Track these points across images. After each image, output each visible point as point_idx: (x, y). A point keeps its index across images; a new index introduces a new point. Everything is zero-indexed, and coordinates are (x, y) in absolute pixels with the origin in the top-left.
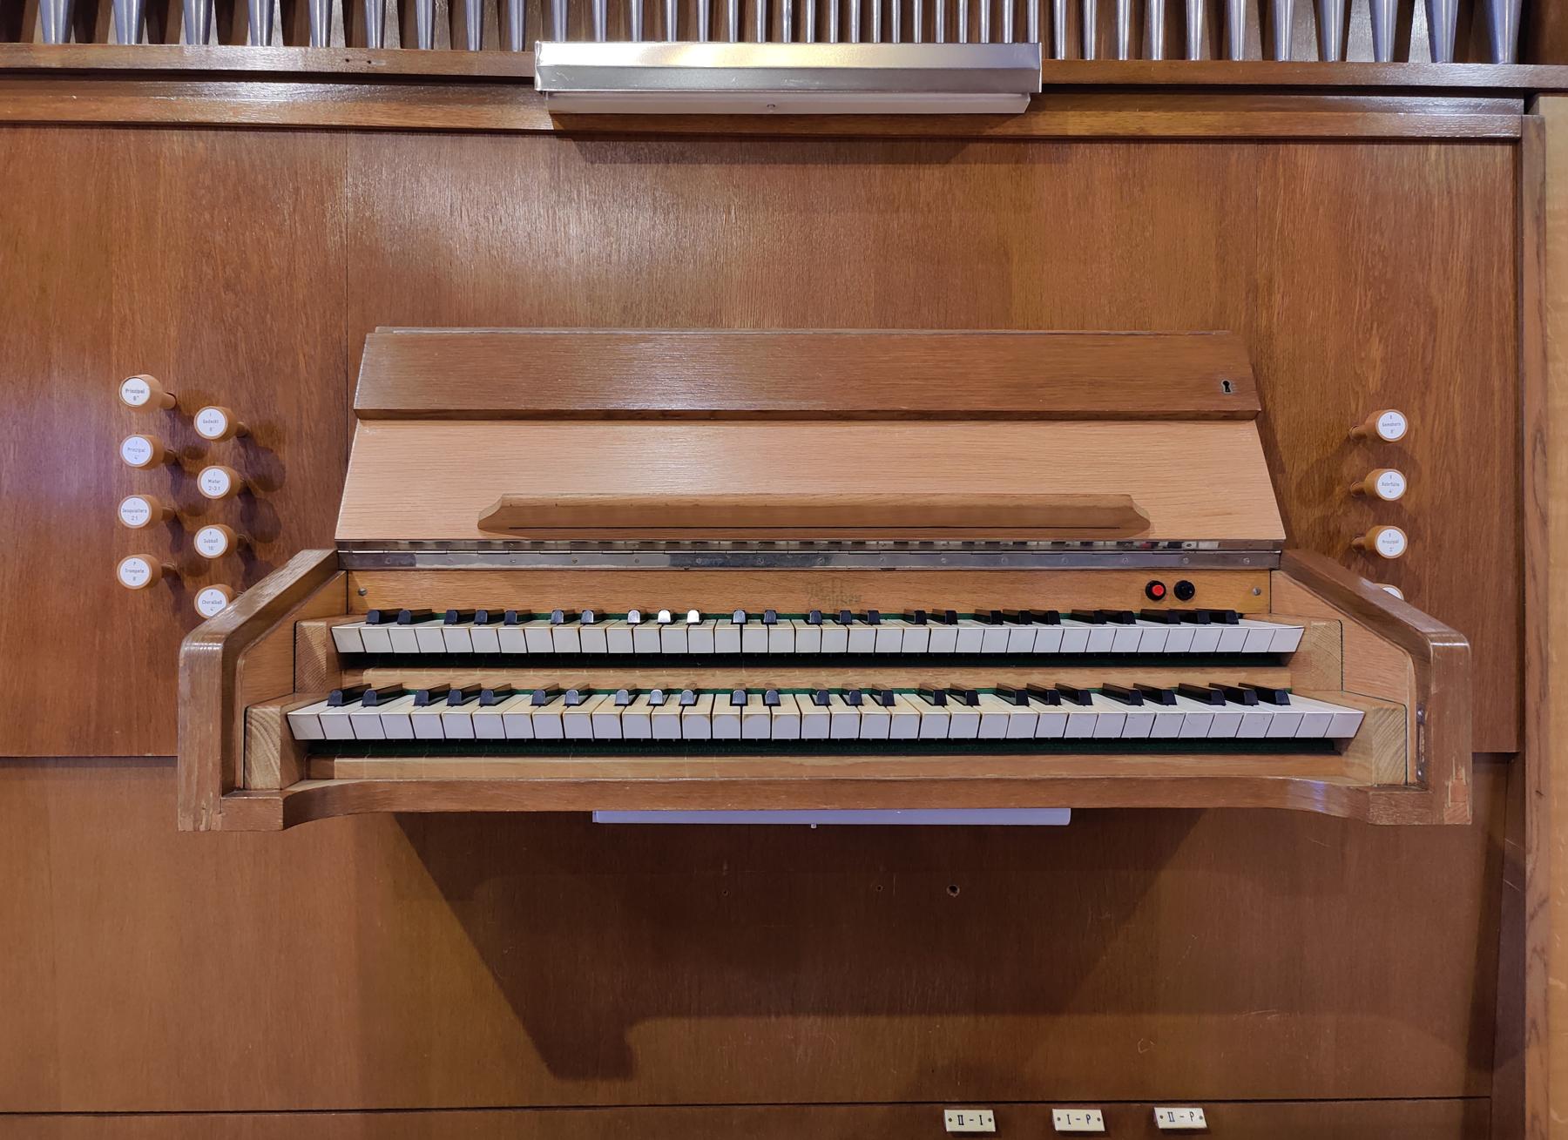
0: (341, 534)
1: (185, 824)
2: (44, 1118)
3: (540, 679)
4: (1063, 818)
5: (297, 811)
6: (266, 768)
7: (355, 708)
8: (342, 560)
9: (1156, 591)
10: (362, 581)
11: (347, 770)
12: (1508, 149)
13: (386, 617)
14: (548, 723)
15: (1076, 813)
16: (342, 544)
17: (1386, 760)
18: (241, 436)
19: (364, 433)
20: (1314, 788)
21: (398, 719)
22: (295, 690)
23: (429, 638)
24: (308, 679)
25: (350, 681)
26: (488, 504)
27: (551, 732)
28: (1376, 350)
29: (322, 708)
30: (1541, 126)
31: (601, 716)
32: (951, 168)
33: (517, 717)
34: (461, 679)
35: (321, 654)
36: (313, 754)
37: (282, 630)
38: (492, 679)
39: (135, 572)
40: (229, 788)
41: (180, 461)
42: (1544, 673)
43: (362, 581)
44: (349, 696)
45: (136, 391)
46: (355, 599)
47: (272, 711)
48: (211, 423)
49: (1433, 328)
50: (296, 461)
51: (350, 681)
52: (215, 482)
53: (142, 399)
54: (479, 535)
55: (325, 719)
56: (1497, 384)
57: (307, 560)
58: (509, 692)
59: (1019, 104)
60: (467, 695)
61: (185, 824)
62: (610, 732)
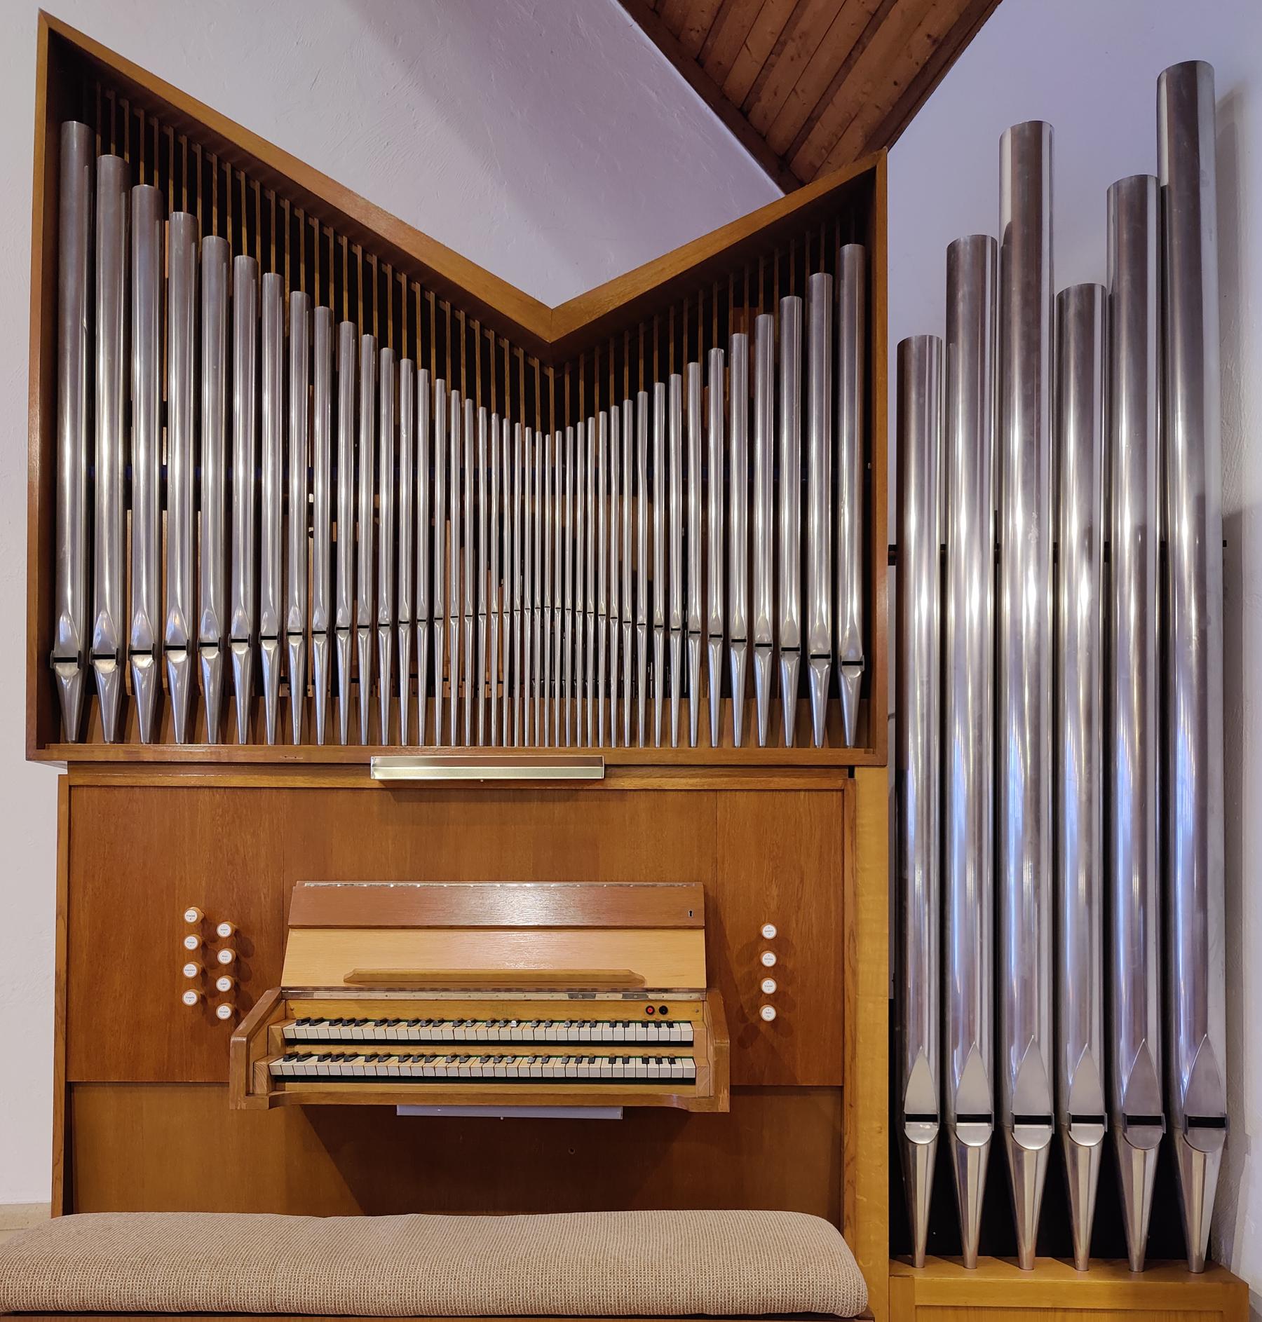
1: (232, 1106)
2: (515, 934)
3: (369, 1050)
4: (617, 1115)
5: (274, 1103)
6: (262, 1086)
7: (294, 1062)
8: (284, 996)
9: (650, 1010)
10: (292, 1004)
11: (290, 1087)
12: (840, 794)
13: (303, 1022)
14: (371, 1069)
15: (627, 1111)
16: (283, 988)
17: (703, 1087)
18: (236, 933)
19: (293, 935)
20: (674, 1097)
21: (311, 1066)
22: (268, 1054)
23: (323, 1031)
24: (273, 1050)
25: (289, 1050)
26: (348, 971)
27: (453, 1073)
28: (775, 891)
29: (280, 1062)
30: (854, 784)
31: (392, 1067)
32: (568, 804)
33: (359, 1067)
34: (336, 1050)
35: (279, 1040)
36: (278, 1080)
37: (264, 1031)
38: (349, 1050)
39: (190, 998)
40: (248, 1094)
42: (854, 1048)
43: (292, 1004)
44: (290, 1057)
45: (191, 915)
46: (289, 1012)
47: (264, 1063)
48: (224, 930)
49: (802, 881)
50: (260, 944)
51: (289, 1050)
52: (225, 957)
53: (194, 919)
54: (343, 985)
55: (282, 1066)
56: (833, 908)
57: (268, 997)
58: (356, 1055)
59: (597, 773)
60: (340, 1056)
61: (232, 1106)
62: (441, 1073)
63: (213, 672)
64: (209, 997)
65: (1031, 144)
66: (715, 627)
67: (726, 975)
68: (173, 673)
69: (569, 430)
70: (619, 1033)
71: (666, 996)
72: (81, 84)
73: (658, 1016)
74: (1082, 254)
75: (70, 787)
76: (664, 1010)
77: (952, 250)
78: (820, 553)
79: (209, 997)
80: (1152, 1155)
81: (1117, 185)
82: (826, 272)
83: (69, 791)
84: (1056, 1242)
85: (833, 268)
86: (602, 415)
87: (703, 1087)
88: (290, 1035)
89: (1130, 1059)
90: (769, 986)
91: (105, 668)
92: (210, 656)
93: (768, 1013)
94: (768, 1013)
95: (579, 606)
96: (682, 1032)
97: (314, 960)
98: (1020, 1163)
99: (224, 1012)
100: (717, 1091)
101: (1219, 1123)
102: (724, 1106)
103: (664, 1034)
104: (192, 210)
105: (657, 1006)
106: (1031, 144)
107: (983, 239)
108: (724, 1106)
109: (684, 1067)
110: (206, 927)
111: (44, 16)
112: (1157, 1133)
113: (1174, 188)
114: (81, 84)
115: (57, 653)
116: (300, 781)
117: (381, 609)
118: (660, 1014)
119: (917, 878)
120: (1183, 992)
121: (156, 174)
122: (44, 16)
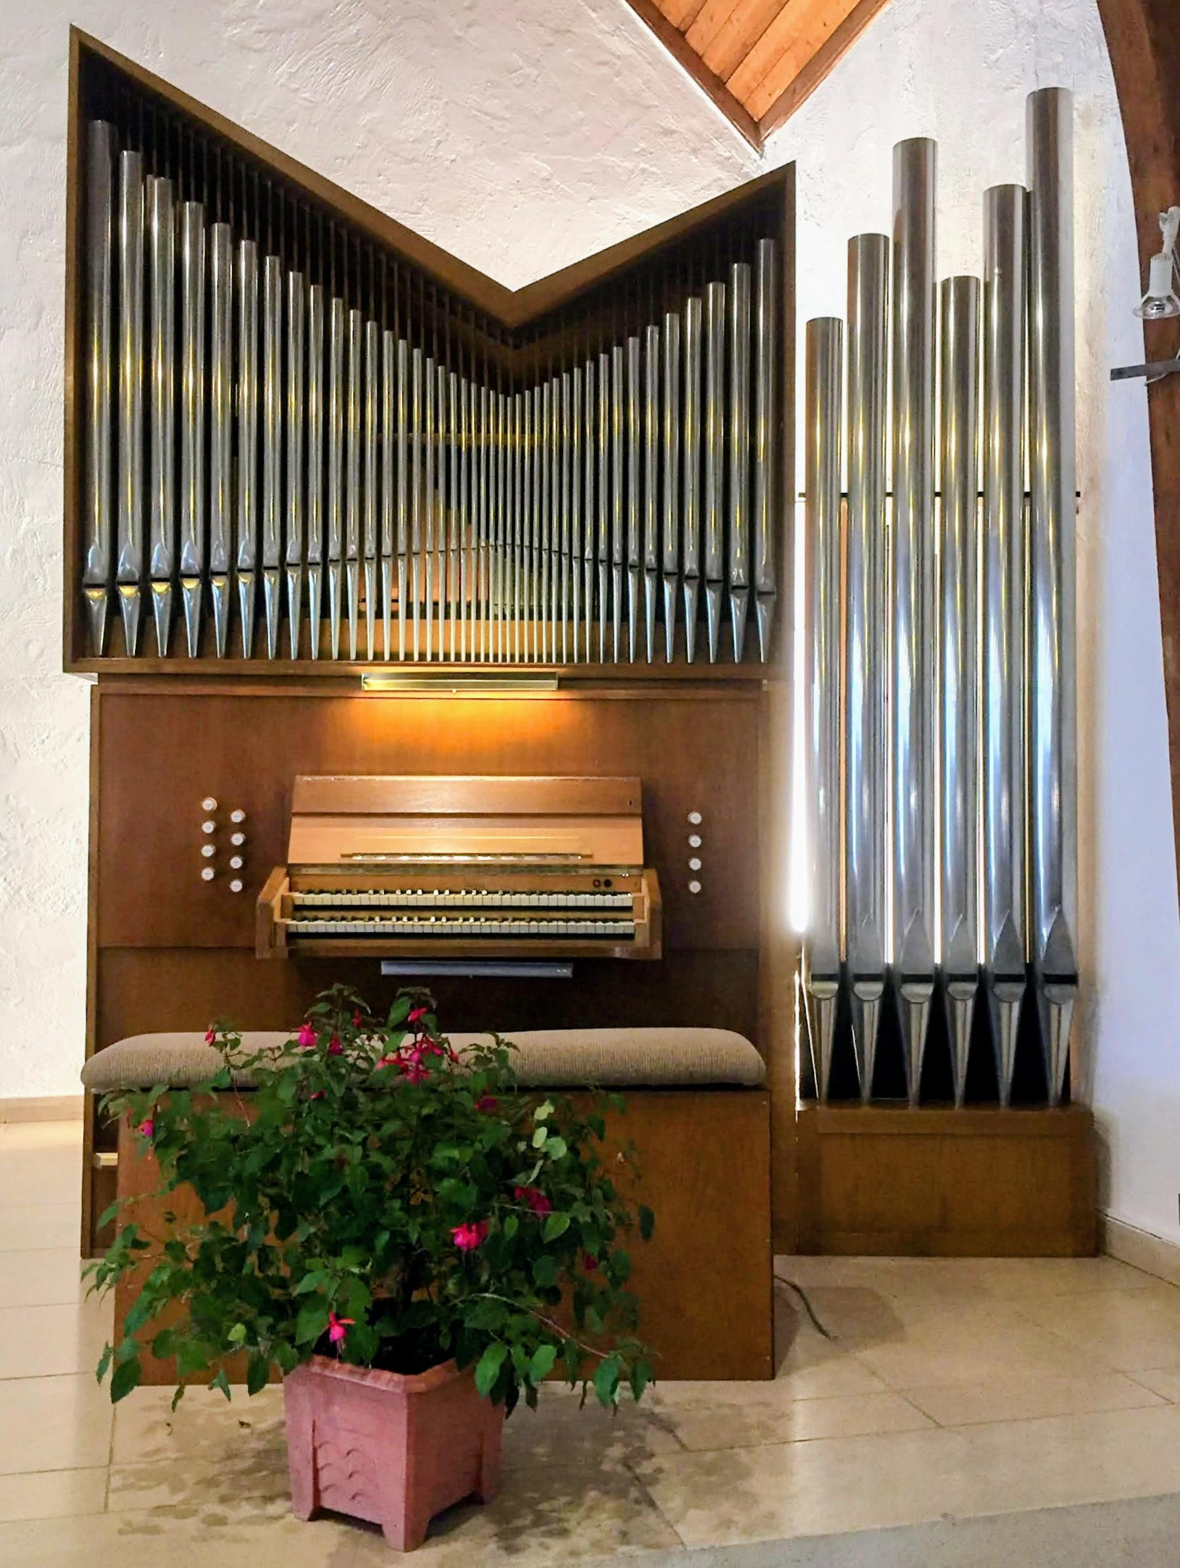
0: (290, 861)
5: (292, 953)
6: (281, 940)
11: (304, 943)
17: (641, 940)
19: (295, 820)
39: (208, 874)
40: (271, 947)
41: (223, 829)
45: (209, 804)
64: (223, 874)
65: (915, 159)
67: (660, 853)
70: (572, 901)
71: (609, 871)
72: (128, 118)
73: (603, 888)
75: (102, 695)
76: (608, 883)
77: (852, 242)
78: (766, 405)
82: (746, 262)
83: (100, 701)
84: (937, 1087)
86: (555, 380)
87: (641, 940)
88: (298, 902)
89: (999, 921)
91: (127, 592)
92: (218, 585)
93: (695, 887)
94: (695, 887)
97: (311, 843)
98: (908, 1013)
99: (236, 886)
100: (652, 942)
102: (658, 954)
103: (608, 901)
104: (174, 177)
105: (602, 880)
106: (915, 159)
107: (871, 241)
108: (658, 954)
110: (220, 815)
111: (74, 30)
112: (1019, 989)
113: (1038, 194)
114: (128, 118)
116: (191, 690)
118: (605, 886)
121: (167, 165)
122: (74, 30)
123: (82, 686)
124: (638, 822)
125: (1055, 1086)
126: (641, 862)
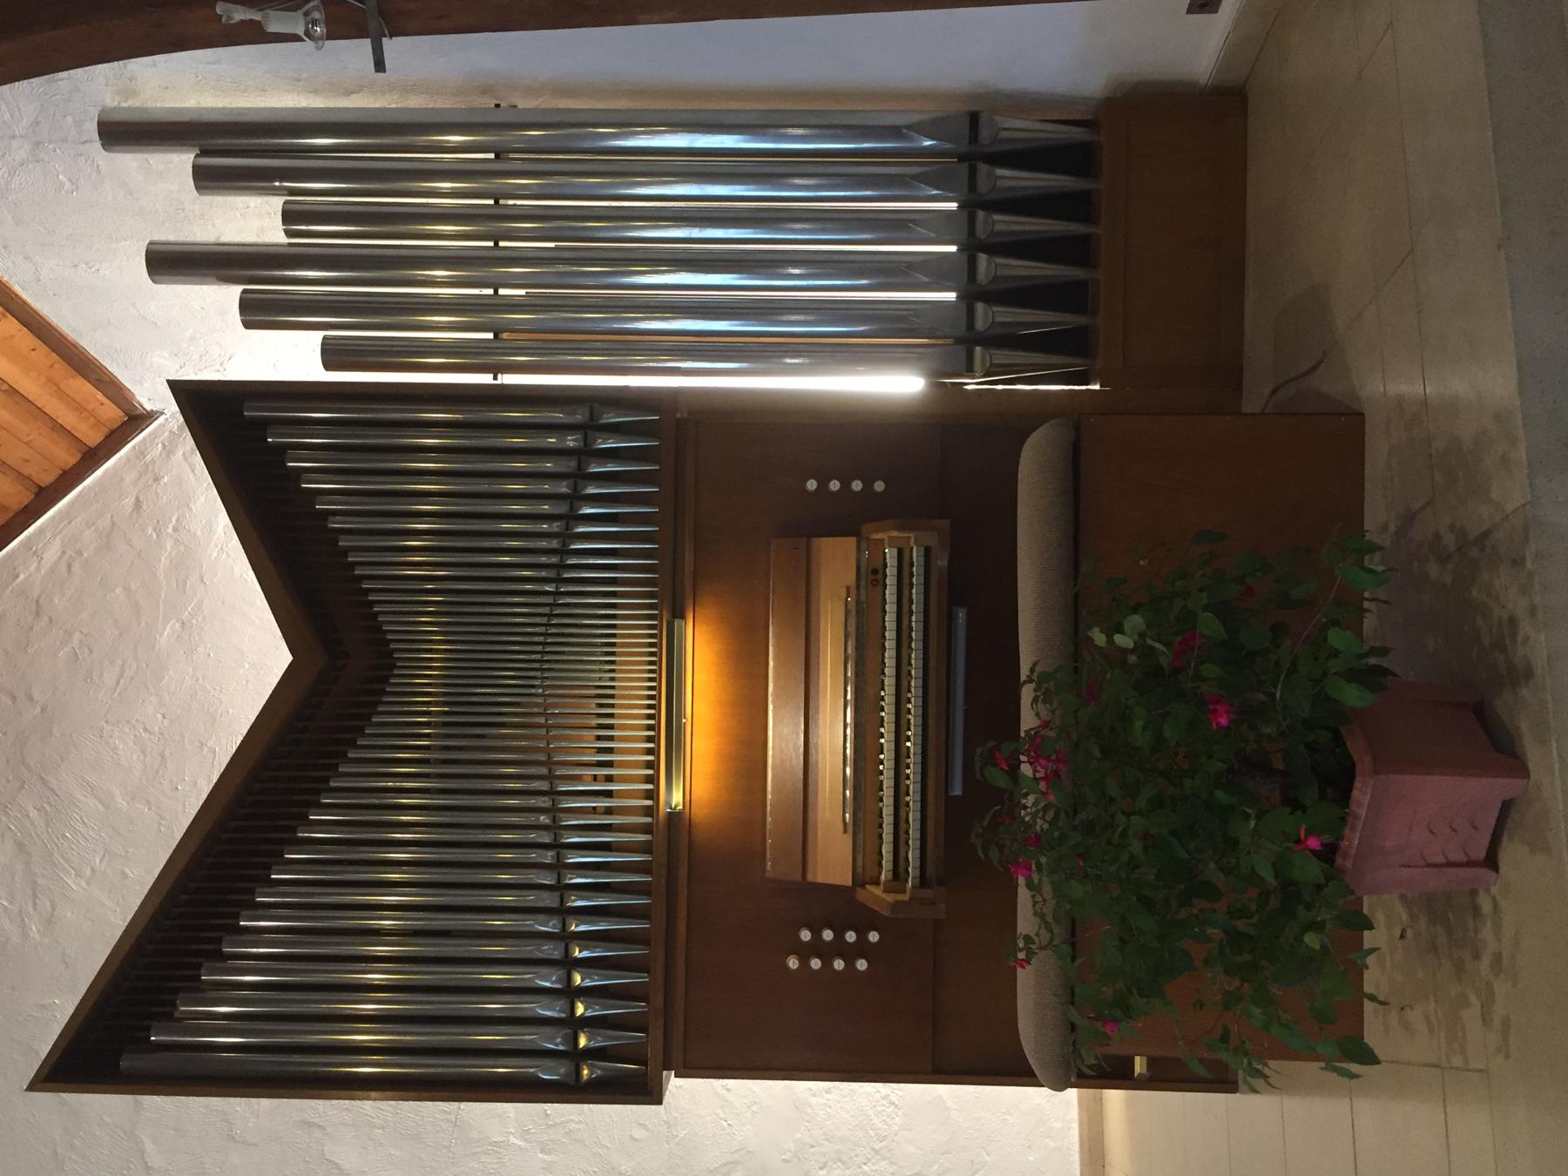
39: (862, 965)
52: (851, 937)
63: (583, 899)
64: (862, 949)
66: (569, 465)
67: (846, 520)
68: (588, 983)
69: (393, 646)
71: (863, 570)
73: (880, 576)
74: (254, 219)
76: (875, 572)
79: (862, 949)
80: (1000, 172)
81: (197, 188)
85: (265, 424)
87: (931, 540)
88: (890, 876)
90: (857, 486)
93: (879, 486)
94: (879, 486)
95: (540, 648)
96: (890, 554)
98: (1005, 278)
101: (974, 118)
102: (945, 524)
103: (891, 572)
104: (176, 991)
105: (871, 577)
108: (945, 524)
109: (916, 555)
110: (805, 953)
111: (32, 1087)
112: (983, 168)
115: (571, 1081)
117: (541, 955)
119: (530, 630)
120: (866, 145)
122: (32, 1087)
123: (677, 1087)
124: (815, 541)
125: (1078, 134)
126: (854, 539)
